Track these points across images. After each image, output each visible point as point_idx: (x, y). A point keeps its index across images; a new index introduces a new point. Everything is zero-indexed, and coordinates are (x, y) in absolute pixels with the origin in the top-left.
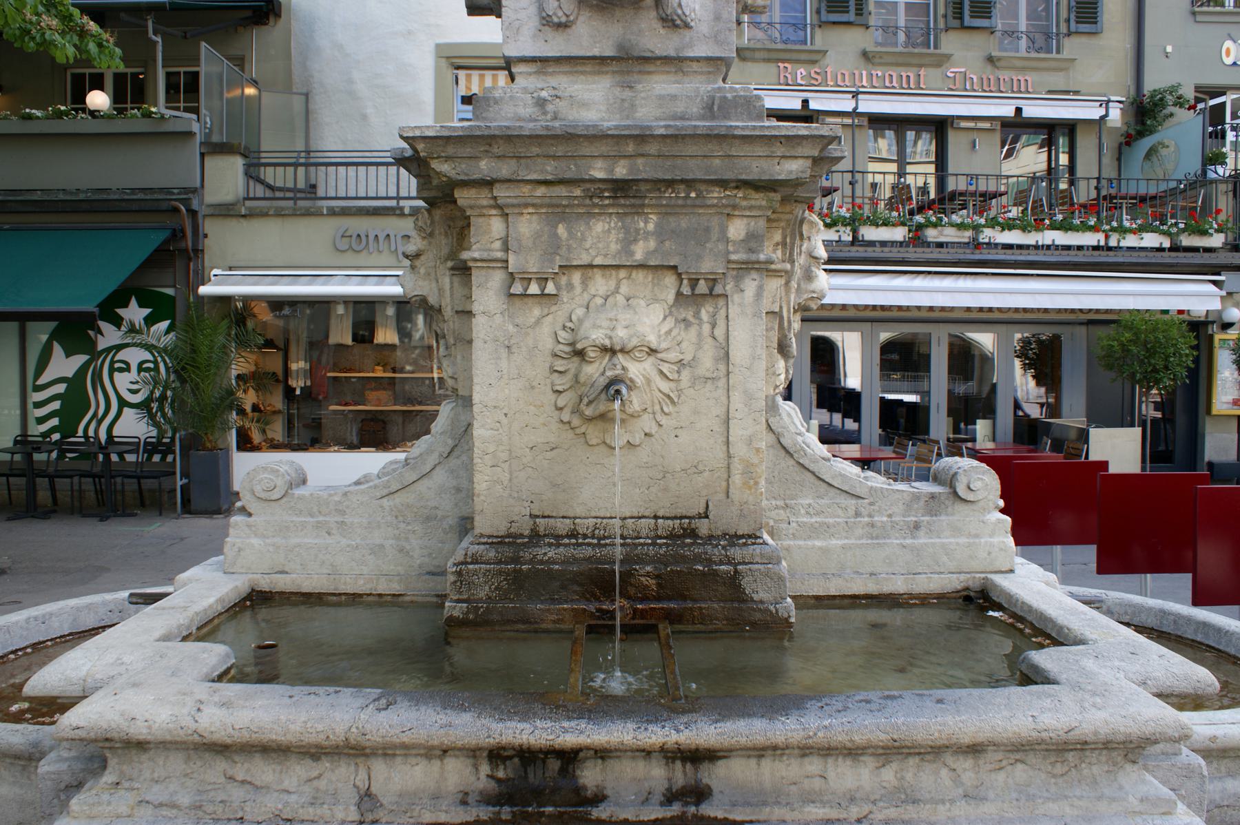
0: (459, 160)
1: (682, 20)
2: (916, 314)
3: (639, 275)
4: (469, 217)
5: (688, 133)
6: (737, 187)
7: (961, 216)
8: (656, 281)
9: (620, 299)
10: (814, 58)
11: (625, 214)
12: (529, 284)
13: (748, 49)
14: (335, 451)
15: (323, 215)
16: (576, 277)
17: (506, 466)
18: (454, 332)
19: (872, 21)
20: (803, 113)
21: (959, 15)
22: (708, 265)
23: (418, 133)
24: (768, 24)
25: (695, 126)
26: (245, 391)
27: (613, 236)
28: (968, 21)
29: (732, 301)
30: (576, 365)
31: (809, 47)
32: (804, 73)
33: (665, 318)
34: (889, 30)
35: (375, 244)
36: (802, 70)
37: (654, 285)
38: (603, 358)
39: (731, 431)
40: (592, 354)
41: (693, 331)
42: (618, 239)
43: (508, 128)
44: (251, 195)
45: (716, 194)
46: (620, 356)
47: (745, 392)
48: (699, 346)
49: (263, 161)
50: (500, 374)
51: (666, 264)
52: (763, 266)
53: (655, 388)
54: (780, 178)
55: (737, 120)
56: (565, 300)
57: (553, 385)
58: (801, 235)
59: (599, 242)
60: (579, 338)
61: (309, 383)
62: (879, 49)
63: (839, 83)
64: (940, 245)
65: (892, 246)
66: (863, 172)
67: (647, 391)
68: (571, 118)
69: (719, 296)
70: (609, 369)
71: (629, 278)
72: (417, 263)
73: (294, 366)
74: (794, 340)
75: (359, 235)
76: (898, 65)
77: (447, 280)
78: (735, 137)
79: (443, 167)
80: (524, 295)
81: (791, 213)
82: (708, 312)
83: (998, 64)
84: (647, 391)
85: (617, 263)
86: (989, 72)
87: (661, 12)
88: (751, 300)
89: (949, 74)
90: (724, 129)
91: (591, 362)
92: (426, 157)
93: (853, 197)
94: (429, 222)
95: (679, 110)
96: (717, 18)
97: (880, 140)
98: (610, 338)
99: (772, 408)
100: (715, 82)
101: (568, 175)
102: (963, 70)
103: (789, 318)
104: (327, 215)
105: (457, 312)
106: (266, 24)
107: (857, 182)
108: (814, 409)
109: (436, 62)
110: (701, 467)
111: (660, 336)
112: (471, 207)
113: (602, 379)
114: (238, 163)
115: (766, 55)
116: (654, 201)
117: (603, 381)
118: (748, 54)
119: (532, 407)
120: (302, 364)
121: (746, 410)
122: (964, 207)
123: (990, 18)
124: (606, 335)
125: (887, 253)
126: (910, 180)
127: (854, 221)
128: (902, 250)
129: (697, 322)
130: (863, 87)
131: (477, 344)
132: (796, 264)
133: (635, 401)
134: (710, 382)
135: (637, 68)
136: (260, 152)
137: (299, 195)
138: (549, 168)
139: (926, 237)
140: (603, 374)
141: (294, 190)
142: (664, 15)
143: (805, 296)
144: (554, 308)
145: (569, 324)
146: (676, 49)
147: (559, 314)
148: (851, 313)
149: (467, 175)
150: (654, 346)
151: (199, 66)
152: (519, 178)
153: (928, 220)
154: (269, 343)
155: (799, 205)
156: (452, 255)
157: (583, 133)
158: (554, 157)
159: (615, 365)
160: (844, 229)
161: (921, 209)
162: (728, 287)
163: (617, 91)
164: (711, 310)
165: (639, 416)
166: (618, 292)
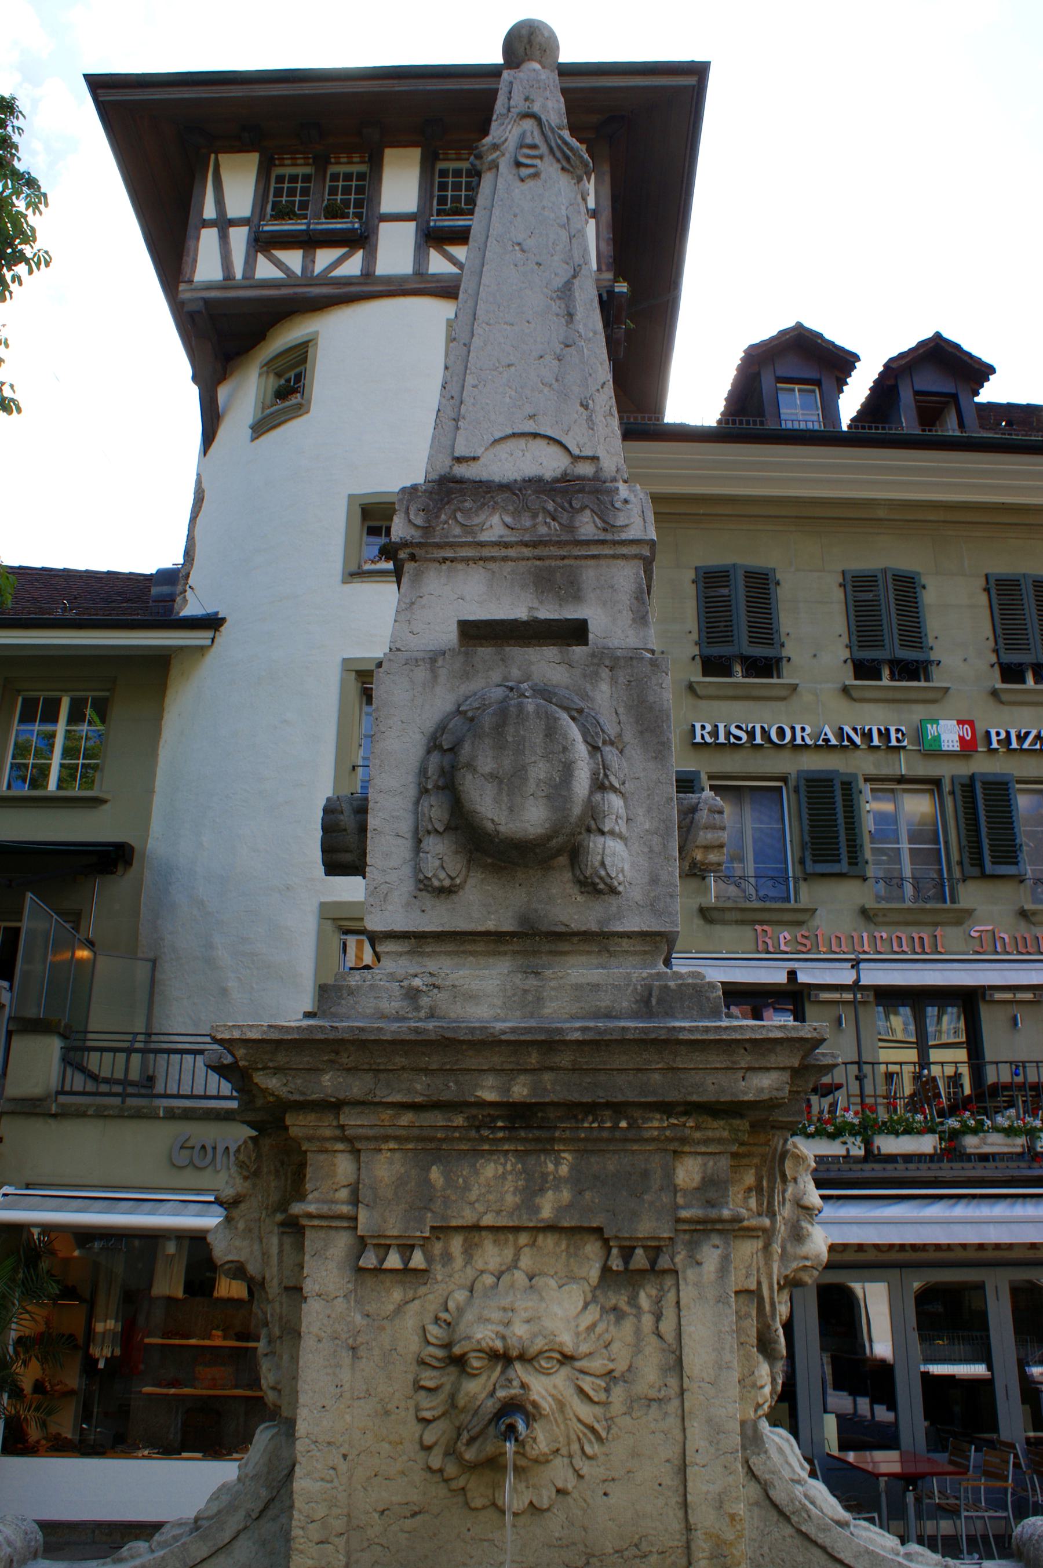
0: (293, 1073)
1: (605, 884)
2: (961, 1255)
3: (548, 1242)
4: (305, 1152)
5: (614, 1037)
6: (686, 1113)
7: (1009, 1118)
8: (572, 1250)
9: (519, 1276)
10: (801, 918)
11: (526, 1152)
12: (387, 1254)
13: (716, 909)
14: (144, 1457)
15: (158, 1117)
16: (456, 1244)
17: (341, 1542)
18: (281, 1318)
19: (871, 871)
20: (790, 988)
21: (978, 861)
22: (647, 1227)
23: (236, 1035)
24: (740, 878)
25: (623, 1028)
26: (25, 1363)
27: (509, 1185)
28: (989, 868)
29: (685, 1279)
30: (453, 1378)
31: (792, 904)
32: (788, 937)
33: (586, 1306)
34: (893, 881)
35: (225, 1160)
36: (786, 934)
37: (569, 1255)
38: (492, 1369)
39: (690, 1484)
40: (476, 1364)
41: (628, 1325)
42: (516, 1188)
43: (362, 1029)
44: (67, 1088)
45: (655, 1123)
46: (518, 1366)
47: (709, 1421)
48: (637, 1349)
49: (90, 1044)
50: (339, 1390)
51: (586, 1224)
52: (728, 1226)
53: (571, 1416)
54: (746, 1098)
55: (684, 1018)
56: (439, 1278)
57: (418, 1409)
58: (784, 1176)
59: (489, 1192)
60: (456, 1337)
61: (118, 1352)
62: (884, 905)
63: (834, 948)
64: (984, 1158)
65: (920, 1162)
66: (873, 1064)
67: (560, 1420)
68: (453, 1015)
69: (664, 1272)
70: (502, 1387)
71: (533, 1244)
72: (236, 1213)
73: (99, 1327)
74: (781, 1331)
75: (203, 1147)
76: (907, 924)
77: (275, 1240)
78: (680, 1042)
79: (271, 1083)
80: (378, 1271)
81: (767, 1143)
82: (649, 1296)
83: (1033, 919)
84: (560, 1420)
85: (516, 1223)
86: (1023, 929)
87: (578, 873)
88: (713, 1277)
89: (973, 934)
90: (663, 1032)
91: (475, 1375)
92: (246, 1068)
93: (862, 1095)
94: (253, 1156)
95: (603, 1004)
96: (654, 880)
97: (892, 1017)
98: (503, 1338)
99: (752, 1440)
100: (654, 965)
101: (445, 1096)
102: (990, 928)
103: (772, 1299)
104: (163, 1118)
105: (287, 1289)
106: (113, 873)
107: (865, 1076)
108: (830, 1391)
109: (320, 925)
110: (645, 1547)
111: (578, 1334)
112: (310, 1139)
113: (490, 1403)
114: (55, 1044)
115: (738, 916)
116: (568, 1134)
117: (490, 1406)
118: (715, 915)
119: (386, 1445)
120: (111, 1324)
121: (712, 1450)
122: (1011, 1104)
123: (1017, 863)
124: (497, 1333)
125: (912, 1171)
126: (936, 1071)
127: (865, 1128)
128: (933, 1166)
129: (634, 1311)
130: (865, 952)
131: (308, 1343)
132: (778, 1218)
133: (541, 1437)
134: (654, 1405)
135: (547, 947)
136: (86, 1032)
137: (130, 1090)
138: (418, 1087)
139: (964, 1147)
140: (492, 1394)
141: (125, 1082)
142: (581, 877)
143: (794, 1265)
144: (422, 1290)
145: (444, 1315)
146: (599, 922)
147: (430, 1298)
148: (871, 1256)
149: (303, 1093)
150: (568, 1350)
151: (20, 921)
152: (377, 1100)
153: (964, 1123)
154: (69, 1292)
155: (778, 1133)
156: (283, 1206)
157: (466, 1038)
158: (426, 1071)
159: (510, 1381)
160: (852, 1139)
161: (953, 1110)
162: (678, 1259)
163: (518, 979)
164: (654, 1292)
165: (548, 1461)
166: (516, 1267)
